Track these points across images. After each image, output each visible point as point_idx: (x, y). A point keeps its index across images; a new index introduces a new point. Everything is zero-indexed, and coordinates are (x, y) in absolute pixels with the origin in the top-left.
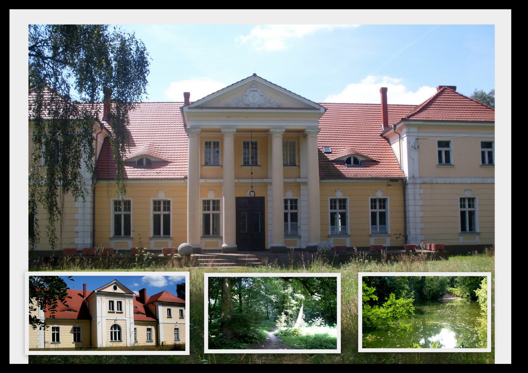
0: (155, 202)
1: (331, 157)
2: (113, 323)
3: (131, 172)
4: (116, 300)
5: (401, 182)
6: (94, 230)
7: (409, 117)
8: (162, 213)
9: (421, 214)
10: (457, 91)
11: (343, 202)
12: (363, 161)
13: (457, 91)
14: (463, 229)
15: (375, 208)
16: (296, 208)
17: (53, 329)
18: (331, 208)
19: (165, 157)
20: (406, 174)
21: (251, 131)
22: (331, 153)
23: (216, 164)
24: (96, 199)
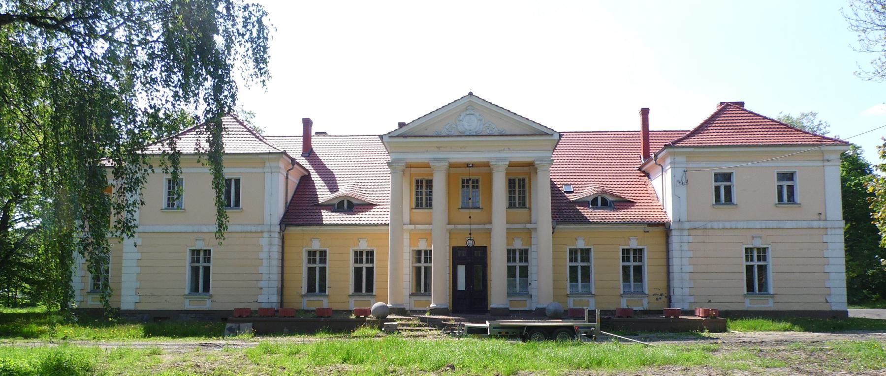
0: (356, 252)
1: (572, 198)
3: (328, 217)
5: (664, 227)
6: (282, 286)
7: (673, 143)
8: (364, 265)
9: (691, 269)
10: (745, 108)
11: (586, 254)
12: (613, 202)
13: (745, 108)
14: (750, 288)
15: (628, 260)
16: (526, 260)
18: (624, 261)
19: (369, 199)
20: (670, 216)
21: (468, 165)
22: (572, 192)
23: (523, 205)
24: (286, 249)
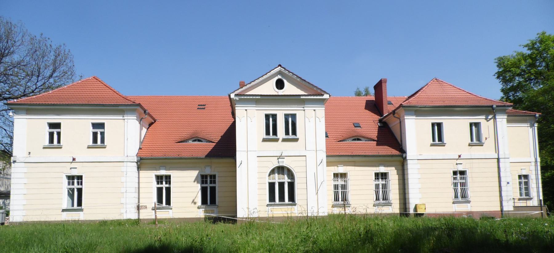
2: (275, 163)
4: (281, 112)
17: (159, 179)
